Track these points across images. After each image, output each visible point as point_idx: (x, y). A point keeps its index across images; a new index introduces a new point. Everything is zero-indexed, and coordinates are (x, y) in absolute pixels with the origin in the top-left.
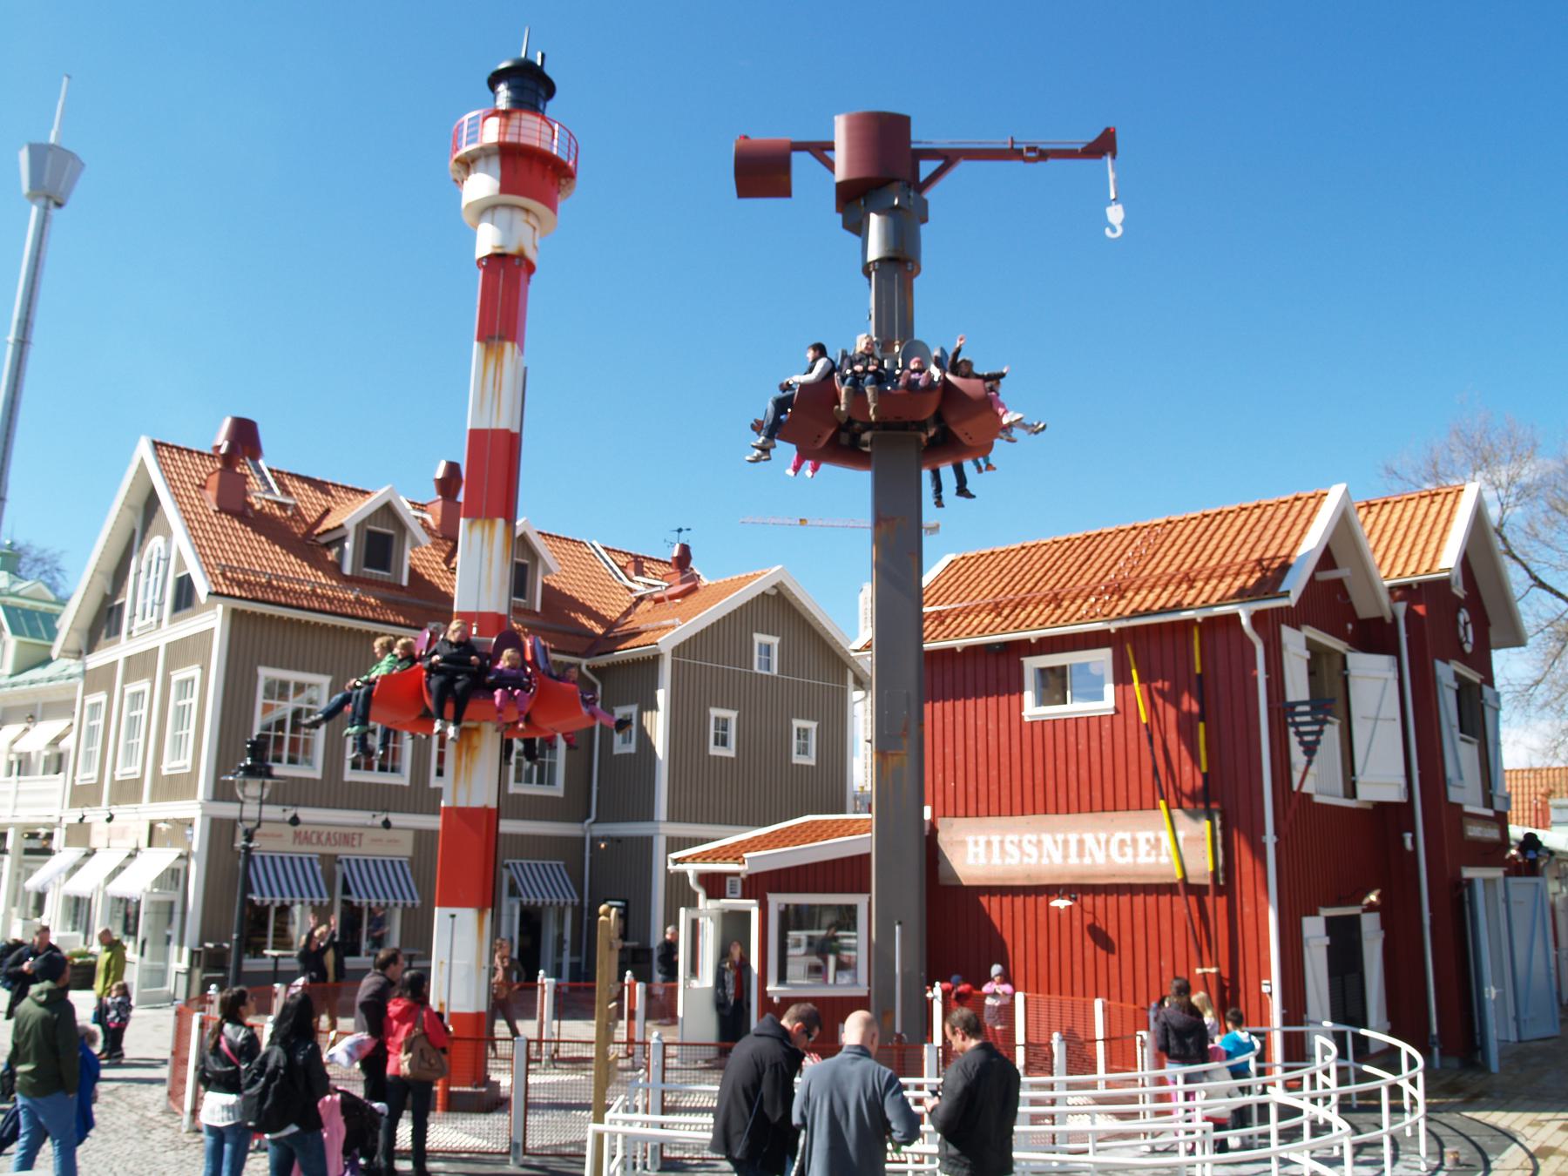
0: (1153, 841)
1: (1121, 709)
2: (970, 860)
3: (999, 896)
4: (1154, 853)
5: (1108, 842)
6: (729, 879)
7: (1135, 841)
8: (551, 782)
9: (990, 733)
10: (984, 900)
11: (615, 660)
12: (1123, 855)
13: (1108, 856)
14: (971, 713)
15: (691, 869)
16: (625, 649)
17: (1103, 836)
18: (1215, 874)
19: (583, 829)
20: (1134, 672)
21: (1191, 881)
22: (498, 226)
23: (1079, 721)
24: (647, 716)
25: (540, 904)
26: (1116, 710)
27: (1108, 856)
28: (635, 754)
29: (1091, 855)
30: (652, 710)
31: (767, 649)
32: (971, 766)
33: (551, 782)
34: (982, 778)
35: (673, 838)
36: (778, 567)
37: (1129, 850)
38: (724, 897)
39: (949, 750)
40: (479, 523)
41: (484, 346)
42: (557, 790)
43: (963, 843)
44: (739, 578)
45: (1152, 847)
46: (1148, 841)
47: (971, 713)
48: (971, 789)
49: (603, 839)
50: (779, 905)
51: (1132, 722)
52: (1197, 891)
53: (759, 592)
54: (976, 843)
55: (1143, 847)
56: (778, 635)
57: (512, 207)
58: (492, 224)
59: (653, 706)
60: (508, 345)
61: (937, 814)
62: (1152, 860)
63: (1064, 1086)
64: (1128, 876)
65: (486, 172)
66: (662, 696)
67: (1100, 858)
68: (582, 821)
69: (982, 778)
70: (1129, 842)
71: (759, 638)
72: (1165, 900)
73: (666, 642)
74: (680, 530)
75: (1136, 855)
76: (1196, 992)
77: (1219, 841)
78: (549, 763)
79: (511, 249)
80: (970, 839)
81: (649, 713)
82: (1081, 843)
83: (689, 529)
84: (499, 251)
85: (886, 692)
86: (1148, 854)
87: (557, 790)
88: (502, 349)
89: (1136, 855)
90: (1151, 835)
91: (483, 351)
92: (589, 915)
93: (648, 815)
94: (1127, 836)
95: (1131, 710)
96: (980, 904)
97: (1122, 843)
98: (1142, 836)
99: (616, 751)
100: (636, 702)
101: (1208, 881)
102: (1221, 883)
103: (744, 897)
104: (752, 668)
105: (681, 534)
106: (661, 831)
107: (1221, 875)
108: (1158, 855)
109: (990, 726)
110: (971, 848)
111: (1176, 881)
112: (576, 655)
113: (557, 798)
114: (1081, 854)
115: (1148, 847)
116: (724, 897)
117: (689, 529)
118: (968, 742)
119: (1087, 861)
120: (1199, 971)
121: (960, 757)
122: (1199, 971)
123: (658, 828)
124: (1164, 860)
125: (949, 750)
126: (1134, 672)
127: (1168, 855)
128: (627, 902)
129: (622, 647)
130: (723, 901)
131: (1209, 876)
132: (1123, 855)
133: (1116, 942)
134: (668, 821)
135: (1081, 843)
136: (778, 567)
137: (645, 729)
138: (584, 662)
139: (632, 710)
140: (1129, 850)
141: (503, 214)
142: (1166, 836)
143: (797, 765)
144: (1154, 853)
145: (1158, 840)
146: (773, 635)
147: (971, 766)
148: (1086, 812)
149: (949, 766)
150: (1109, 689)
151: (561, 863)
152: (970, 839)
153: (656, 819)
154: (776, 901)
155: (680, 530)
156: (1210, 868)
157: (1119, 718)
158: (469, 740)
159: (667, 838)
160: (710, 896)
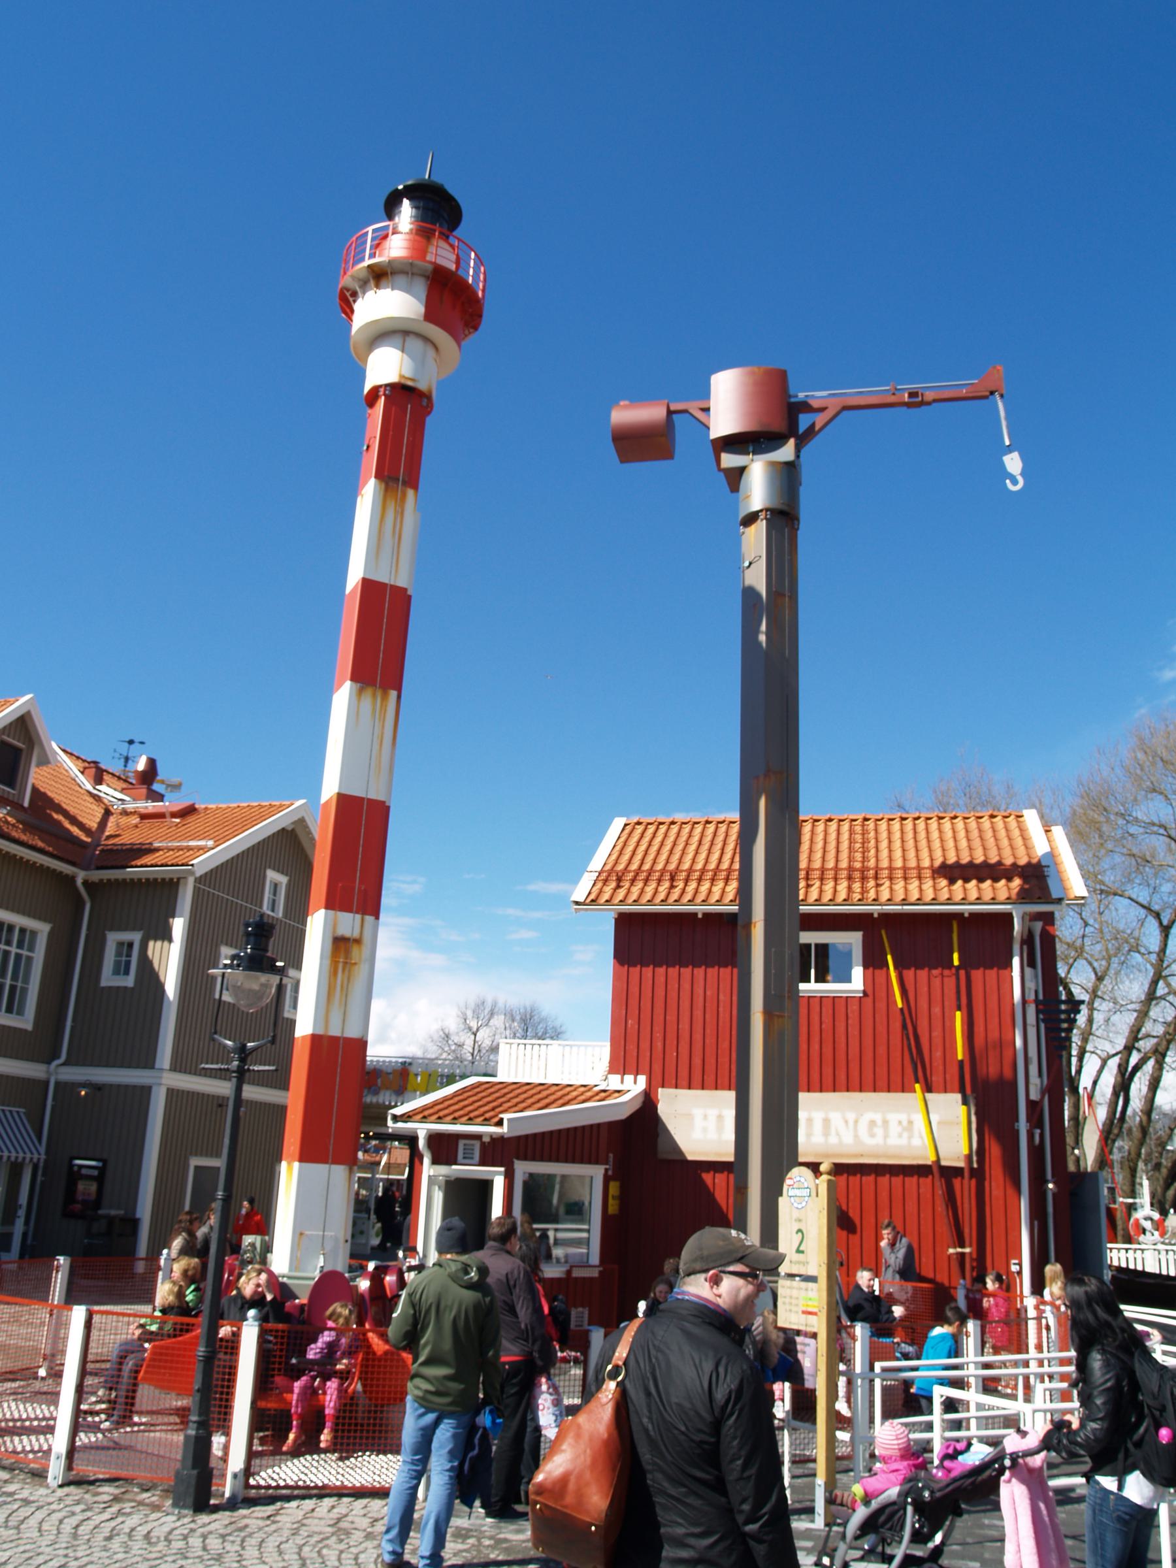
0: (905, 1123)
1: (870, 992)
2: (697, 1134)
3: (901, 1176)
4: (905, 1135)
5: (856, 1122)
6: (461, 1143)
7: (886, 1123)
8: (20, 1012)
9: (721, 1005)
10: (707, 1177)
11: (128, 877)
12: (872, 1135)
13: (856, 1136)
14: (673, 985)
15: (422, 1130)
16: (142, 866)
17: (851, 1116)
18: (969, 1158)
19: (48, 1072)
20: (889, 958)
21: (943, 1163)
22: (410, 356)
23: (811, 1000)
24: (154, 949)
25: (20, 1160)
26: (864, 992)
27: (856, 1136)
28: (132, 989)
29: (838, 1134)
30: (163, 939)
31: (276, 886)
32: (698, 1037)
33: (20, 1012)
34: (711, 1051)
35: (173, 1090)
36: (302, 802)
37: (879, 1131)
38: (455, 1162)
39: (672, 1018)
40: (369, 692)
41: (383, 486)
42: (26, 1021)
43: (690, 1117)
44: (217, 809)
45: (905, 1129)
46: (900, 1122)
47: (673, 985)
48: (697, 1061)
49: (84, 1085)
50: (524, 1173)
51: (881, 1005)
52: (949, 1173)
53: (280, 828)
54: (705, 1117)
55: (894, 1129)
56: (287, 875)
57: (426, 339)
58: (403, 351)
59: (167, 936)
60: (410, 493)
61: (654, 1083)
62: (903, 1141)
63: (980, 1366)
64: (877, 1156)
65: (407, 290)
66: (178, 926)
67: (848, 1139)
68: (49, 1063)
69: (711, 1051)
70: (879, 1123)
71: (272, 875)
72: (912, 1182)
73: (202, 862)
74: (131, 742)
75: (886, 1136)
76: (391, 1275)
77: (974, 1126)
78: (22, 988)
79: (422, 386)
80: (698, 1113)
81: (159, 943)
82: (827, 1122)
83: (142, 743)
84: (410, 383)
85: (773, 950)
86: (900, 1136)
87: (26, 1021)
88: (404, 495)
89: (886, 1136)
90: (903, 1117)
91: (382, 493)
92: (43, 1175)
93: (147, 1061)
94: (878, 1117)
95: (882, 994)
96: (702, 1183)
97: (872, 1123)
98: (894, 1118)
99: (104, 983)
100: (140, 930)
101: (961, 1164)
102: (975, 1165)
103: (482, 1163)
104: (261, 907)
105: (133, 746)
106: (164, 1081)
107: (975, 1158)
108: (910, 1137)
109: (722, 997)
110: (698, 1122)
111: (929, 1163)
112: (73, 864)
113: (26, 1031)
114: (826, 1131)
115: (899, 1129)
116: (456, 1164)
117: (142, 743)
118: (695, 1013)
119: (833, 1140)
120: (967, 1250)
121: (685, 1026)
122: (967, 1250)
123: (161, 1078)
124: (916, 1142)
125: (672, 1018)
126: (889, 958)
127: (921, 1137)
128: (104, 1161)
129: (139, 862)
130: (454, 1167)
131: (963, 1158)
132: (872, 1135)
133: (857, 1222)
134: (170, 1070)
135: (827, 1122)
136: (302, 802)
137: (150, 963)
138: (81, 876)
139: (136, 937)
140: (879, 1131)
141: (414, 344)
142: (919, 1119)
143: (287, 1019)
144: (905, 1135)
145: (910, 1122)
146: (282, 873)
147: (698, 1037)
148: (869, 1091)
149: (672, 1035)
150: (858, 973)
151: (22, 1110)
152: (698, 1113)
153: (157, 1066)
154: (523, 1168)
155: (131, 742)
156: (966, 1151)
157: (869, 1000)
158: (348, 953)
159: (168, 1089)
160: (435, 1161)
